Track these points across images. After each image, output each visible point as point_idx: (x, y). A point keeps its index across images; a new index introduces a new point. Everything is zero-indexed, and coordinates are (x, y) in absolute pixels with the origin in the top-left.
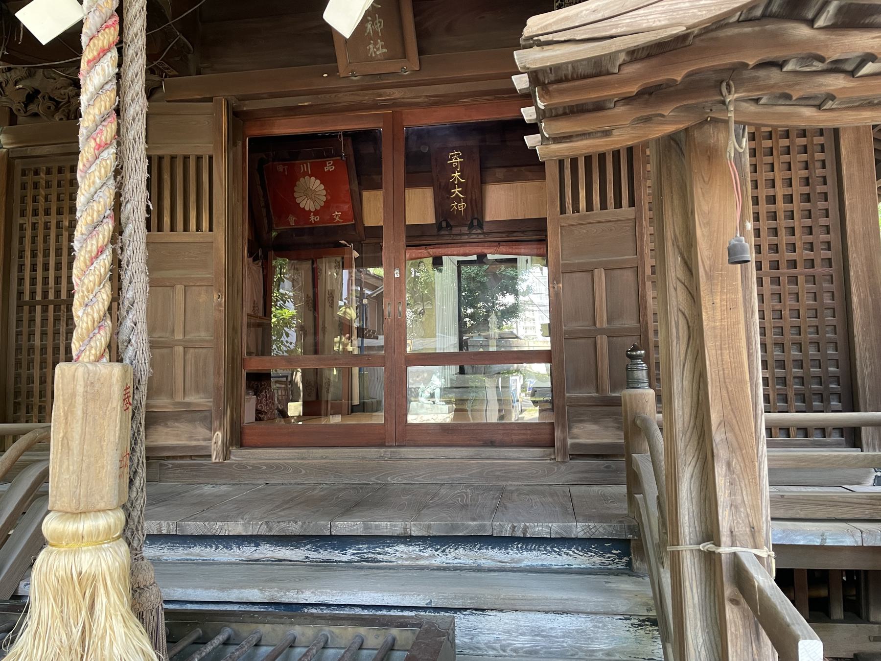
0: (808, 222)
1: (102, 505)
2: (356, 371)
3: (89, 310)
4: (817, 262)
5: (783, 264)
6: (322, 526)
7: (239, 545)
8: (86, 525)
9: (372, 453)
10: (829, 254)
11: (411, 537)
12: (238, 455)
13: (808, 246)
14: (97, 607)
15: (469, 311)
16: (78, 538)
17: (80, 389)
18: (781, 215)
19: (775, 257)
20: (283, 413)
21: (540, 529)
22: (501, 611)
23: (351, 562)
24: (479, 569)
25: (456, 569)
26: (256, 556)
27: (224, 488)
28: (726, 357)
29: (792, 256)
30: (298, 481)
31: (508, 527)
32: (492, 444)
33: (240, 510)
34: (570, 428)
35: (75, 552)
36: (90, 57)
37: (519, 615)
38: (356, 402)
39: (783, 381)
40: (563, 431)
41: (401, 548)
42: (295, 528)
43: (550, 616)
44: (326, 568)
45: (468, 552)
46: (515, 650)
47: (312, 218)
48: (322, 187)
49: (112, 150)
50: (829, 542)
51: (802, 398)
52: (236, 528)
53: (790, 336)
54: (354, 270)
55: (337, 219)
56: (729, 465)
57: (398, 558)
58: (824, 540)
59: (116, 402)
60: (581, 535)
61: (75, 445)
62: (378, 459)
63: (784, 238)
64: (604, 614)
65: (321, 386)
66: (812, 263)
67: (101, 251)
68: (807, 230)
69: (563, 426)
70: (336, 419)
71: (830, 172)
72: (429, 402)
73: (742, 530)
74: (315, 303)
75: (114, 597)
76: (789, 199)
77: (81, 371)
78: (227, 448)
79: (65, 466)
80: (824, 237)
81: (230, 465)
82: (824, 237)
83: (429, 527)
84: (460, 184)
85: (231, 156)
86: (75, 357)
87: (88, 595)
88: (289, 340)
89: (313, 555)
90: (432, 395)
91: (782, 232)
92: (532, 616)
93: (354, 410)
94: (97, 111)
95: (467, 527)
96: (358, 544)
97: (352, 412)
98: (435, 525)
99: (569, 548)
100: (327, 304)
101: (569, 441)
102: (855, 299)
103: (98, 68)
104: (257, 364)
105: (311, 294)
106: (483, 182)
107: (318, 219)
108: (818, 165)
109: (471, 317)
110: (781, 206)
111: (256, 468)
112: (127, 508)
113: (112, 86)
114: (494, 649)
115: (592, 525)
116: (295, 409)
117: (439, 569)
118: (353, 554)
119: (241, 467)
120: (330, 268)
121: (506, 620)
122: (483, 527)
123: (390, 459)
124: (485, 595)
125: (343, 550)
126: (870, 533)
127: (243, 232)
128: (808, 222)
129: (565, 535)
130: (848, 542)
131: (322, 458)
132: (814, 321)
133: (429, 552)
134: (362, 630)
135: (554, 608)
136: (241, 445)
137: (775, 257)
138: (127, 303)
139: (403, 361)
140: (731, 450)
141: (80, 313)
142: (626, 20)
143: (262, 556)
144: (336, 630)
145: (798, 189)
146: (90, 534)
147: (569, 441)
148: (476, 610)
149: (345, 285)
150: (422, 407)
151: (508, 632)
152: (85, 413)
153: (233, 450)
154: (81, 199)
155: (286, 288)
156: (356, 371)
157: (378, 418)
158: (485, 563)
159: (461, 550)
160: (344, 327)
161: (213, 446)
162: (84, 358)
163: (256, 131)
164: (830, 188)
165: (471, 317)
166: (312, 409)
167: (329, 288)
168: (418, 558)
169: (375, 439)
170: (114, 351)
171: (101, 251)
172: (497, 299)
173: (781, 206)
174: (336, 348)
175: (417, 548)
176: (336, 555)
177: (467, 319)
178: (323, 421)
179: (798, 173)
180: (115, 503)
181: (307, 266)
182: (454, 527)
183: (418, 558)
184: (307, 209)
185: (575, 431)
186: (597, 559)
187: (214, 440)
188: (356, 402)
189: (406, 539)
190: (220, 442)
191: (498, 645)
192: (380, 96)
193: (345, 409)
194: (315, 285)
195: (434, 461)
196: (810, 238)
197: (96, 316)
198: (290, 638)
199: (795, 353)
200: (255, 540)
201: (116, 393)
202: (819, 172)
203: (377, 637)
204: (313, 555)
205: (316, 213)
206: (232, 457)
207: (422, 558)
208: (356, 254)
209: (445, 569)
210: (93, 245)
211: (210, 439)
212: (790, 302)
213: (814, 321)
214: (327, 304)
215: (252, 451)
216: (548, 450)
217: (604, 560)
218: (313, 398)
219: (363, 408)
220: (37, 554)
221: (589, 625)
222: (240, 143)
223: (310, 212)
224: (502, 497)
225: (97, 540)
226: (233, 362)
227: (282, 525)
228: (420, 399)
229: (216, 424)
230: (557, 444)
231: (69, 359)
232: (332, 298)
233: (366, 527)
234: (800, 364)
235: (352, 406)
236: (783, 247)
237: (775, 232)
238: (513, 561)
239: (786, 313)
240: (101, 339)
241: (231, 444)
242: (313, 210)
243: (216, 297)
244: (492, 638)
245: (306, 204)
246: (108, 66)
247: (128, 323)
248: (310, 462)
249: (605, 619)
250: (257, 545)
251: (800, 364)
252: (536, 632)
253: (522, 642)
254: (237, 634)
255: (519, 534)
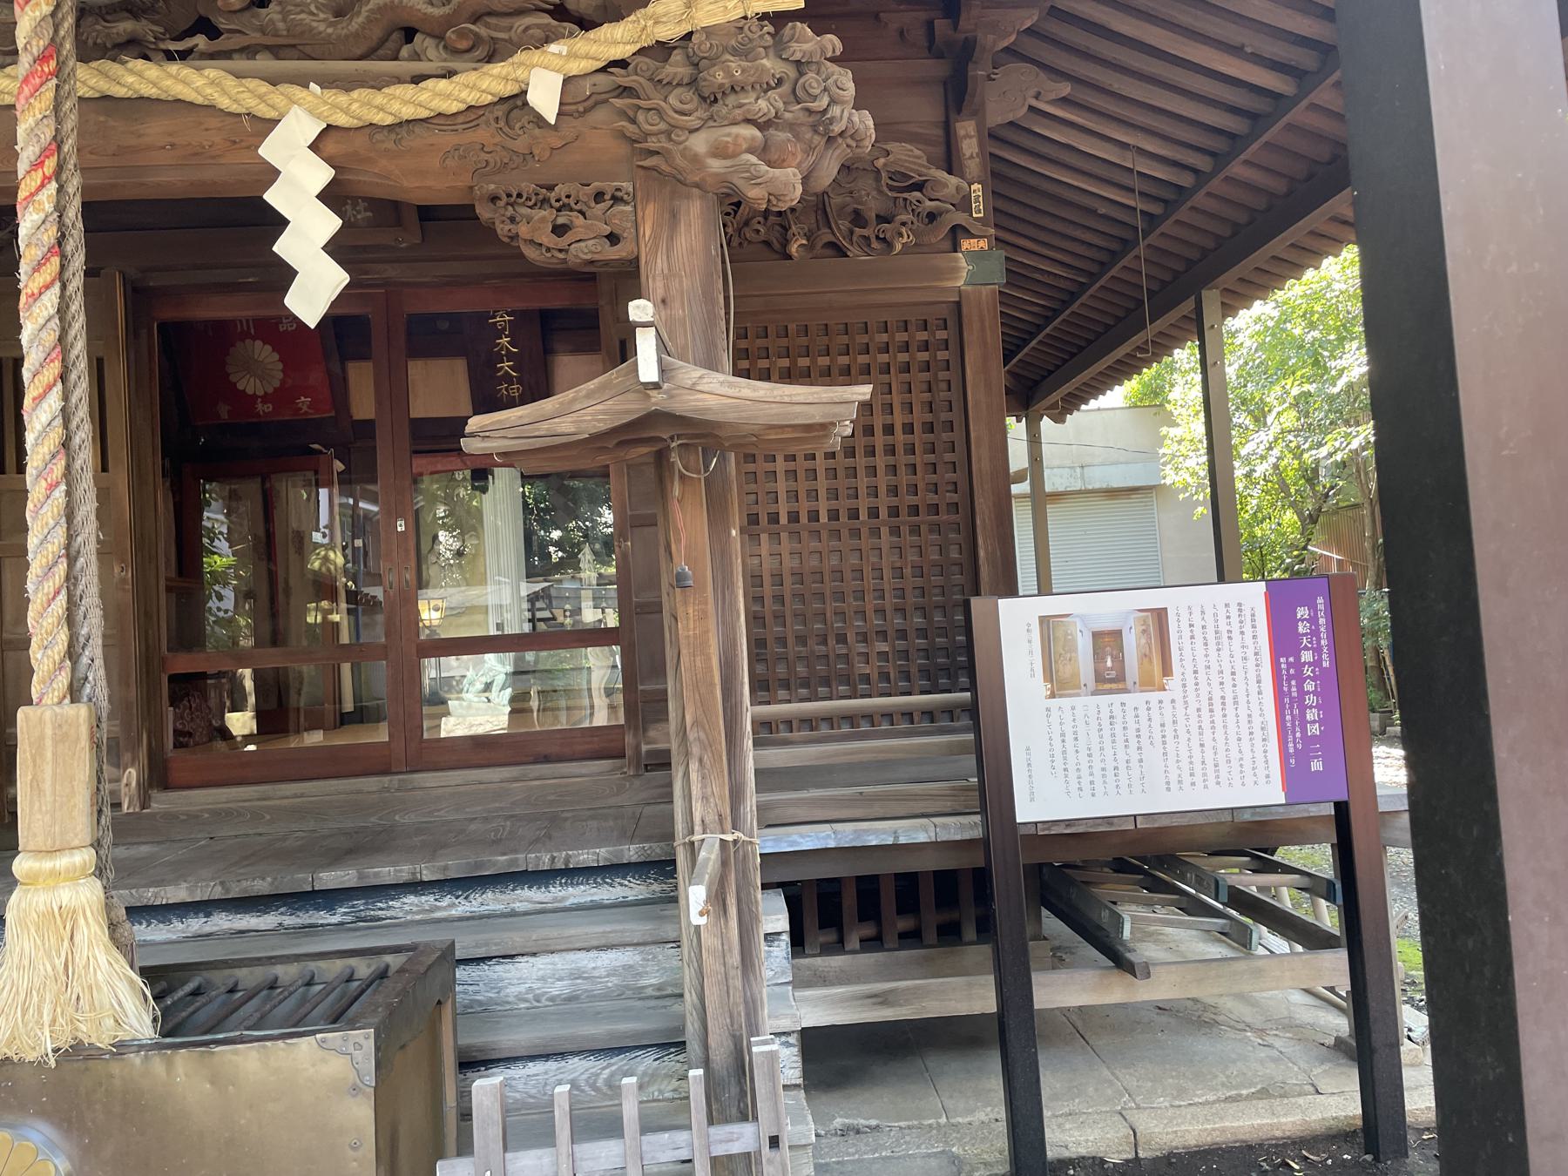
0: (931, 458)
1: (76, 843)
2: (346, 668)
3: (49, 652)
4: (943, 508)
5: (904, 511)
6: (302, 880)
7: (181, 918)
8: (62, 862)
9: (371, 783)
10: (955, 498)
11: (422, 883)
12: (162, 802)
13: (932, 487)
14: (77, 938)
15: (556, 534)
16: (54, 874)
17: (49, 732)
18: (900, 449)
19: (894, 501)
20: (225, 733)
21: (585, 857)
22: (534, 954)
23: (342, 924)
24: (513, 914)
25: (482, 917)
26: (207, 929)
27: (145, 849)
28: (698, 664)
29: (913, 500)
30: (260, 830)
31: (546, 858)
32: (547, 759)
33: (178, 872)
34: (645, 730)
35: (54, 888)
36: (35, 394)
37: (556, 958)
38: (348, 706)
39: (905, 654)
40: (635, 735)
41: (411, 899)
42: (261, 886)
43: (593, 954)
44: (307, 935)
45: (498, 895)
46: (552, 999)
47: (260, 406)
48: (276, 356)
49: (63, 487)
50: (902, 840)
51: (926, 673)
52: (178, 893)
53: (912, 599)
54: (336, 490)
55: (305, 408)
56: (701, 760)
57: (407, 913)
58: (896, 838)
59: (84, 742)
60: (634, 859)
61: (47, 786)
62: (380, 791)
63: (904, 478)
64: (654, 943)
65: (288, 687)
66: (935, 509)
67: (57, 593)
68: (930, 468)
69: (636, 729)
70: (315, 738)
71: (954, 395)
72: (477, 701)
73: (711, 818)
74: (272, 547)
75: (95, 928)
76: (909, 428)
77: (48, 714)
78: (146, 792)
79: (36, 807)
80: (950, 476)
81: (153, 815)
82: (950, 476)
83: (446, 868)
84: (510, 356)
85: (132, 356)
86: (35, 700)
87: (68, 928)
88: (223, 605)
89: (289, 921)
90: (488, 687)
91: (902, 470)
92: (571, 956)
93: (344, 720)
94: (46, 450)
95: (495, 864)
96: (352, 899)
97: (342, 724)
98: (454, 865)
99: (624, 878)
100: (292, 550)
101: (644, 748)
102: (982, 553)
103: (45, 405)
104: (184, 663)
105: (261, 532)
106: (548, 352)
107: (269, 408)
108: (944, 386)
109: (559, 544)
110: (900, 437)
111: (193, 818)
112: (97, 845)
113: (59, 421)
114: (526, 1001)
115: (647, 846)
116: (241, 722)
117: (461, 919)
118: (345, 914)
119: (170, 817)
120: (294, 486)
121: (541, 964)
122: (514, 862)
123: (398, 790)
124: (513, 939)
125: (331, 909)
126: (945, 826)
127: (154, 462)
128: (931, 458)
129: (615, 861)
130: (922, 838)
131: (295, 796)
132: (919, 581)
133: (447, 900)
134: (353, 962)
135: (595, 943)
136: (166, 786)
137: (894, 501)
138: (82, 640)
139: (414, 650)
140: (703, 748)
141: (39, 656)
142: (545, 426)
143: (215, 929)
144: (322, 964)
145: (919, 417)
146: (67, 871)
147: (644, 748)
148: (504, 957)
149: (324, 518)
150: (469, 707)
151: (543, 979)
152: (54, 754)
153: (155, 793)
154: (32, 541)
155: (214, 517)
156: (346, 668)
157: (380, 734)
158: (520, 906)
159: (489, 894)
160: (324, 588)
161: (124, 790)
162: (47, 700)
163: (170, 314)
164: (956, 416)
165: (559, 544)
166: (272, 721)
167: (294, 525)
168: (434, 909)
169: (375, 764)
170: (74, 693)
171: (57, 593)
172: (600, 515)
173: (900, 437)
174: (310, 620)
175: (431, 898)
176: (323, 917)
177: (552, 549)
178: (293, 743)
179: (919, 397)
180: (89, 842)
181: (252, 487)
182: (478, 865)
183: (434, 909)
184: (250, 391)
185: (652, 734)
186: (656, 887)
187: (125, 781)
188: (348, 706)
189: (416, 886)
190: (134, 784)
191: (530, 996)
192: (366, 273)
193: (330, 719)
194: (268, 516)
195: (462, 789)
196: (933, 478)
197: (57, 658)
198: (271, 977)
199: (918, 620)
200: (204, 907)
201: (84, 731)
202: (944, 395)
203: (369, 966)
204: (289, 921)
205: (266, 398)
206: (154, 805)
207: (439, 909)
208: (339, 466)
209: (468, 919)
210: (49, 586)
211: (118, 780)
212: (912, 557)
213: (919, 581)
214: (292, 550)
215: (184, 793)
216: (618, 762)
217: (665, 887)
218: (272, 704)
219: (362, 716)
220: (11, 892)
221: (638, 958)
222: (144, 332)
223: (255, 397)
224: (551, 822)
225: (72, 876)
226: (149, 663)
227: (244, 884)
228: (464, 695)
229: (127, 757)
230: (628, 752)
231: (30, 702)
232: (301, 543)
233: (361, 876)
234: (923, 633)
235: (342, 715)
236: (903, 489)
237: (893, 469)
238: (555, 900)
239: (908, 571)
240: (63, 680)
241: (151, 786)
242: (260, 393)
243: (117, 570)
244: (522, 988)
245: (249, 385)
246: (54, 401)
247: (85, 660)
248: (278, 802)
249: (656, 949)
250: (208, 915)
251: (923, 633)
252: (576, 975)
253: (558, 988)
254: (208, 982)
255: (560, 865)
